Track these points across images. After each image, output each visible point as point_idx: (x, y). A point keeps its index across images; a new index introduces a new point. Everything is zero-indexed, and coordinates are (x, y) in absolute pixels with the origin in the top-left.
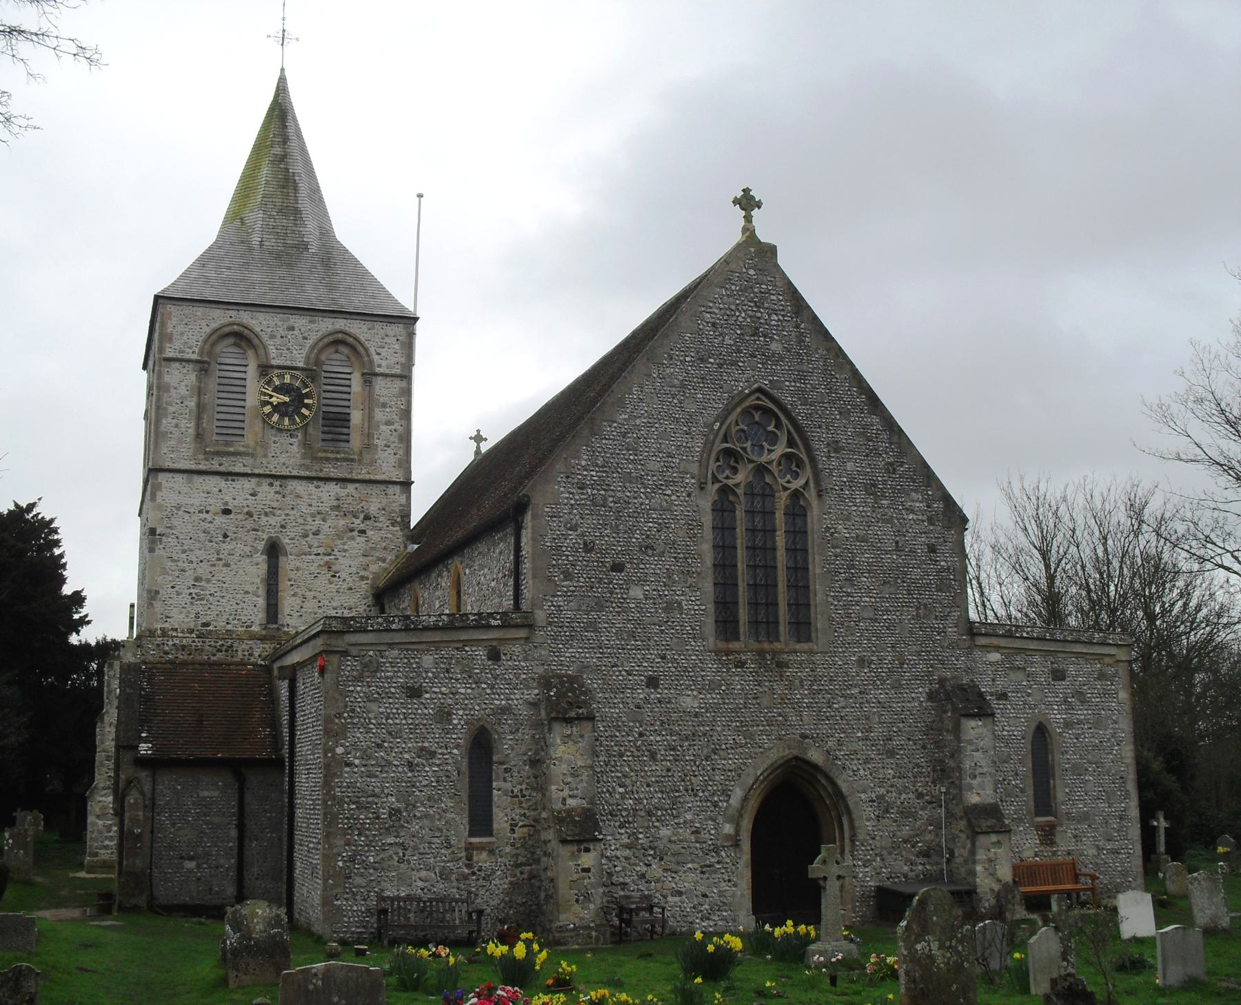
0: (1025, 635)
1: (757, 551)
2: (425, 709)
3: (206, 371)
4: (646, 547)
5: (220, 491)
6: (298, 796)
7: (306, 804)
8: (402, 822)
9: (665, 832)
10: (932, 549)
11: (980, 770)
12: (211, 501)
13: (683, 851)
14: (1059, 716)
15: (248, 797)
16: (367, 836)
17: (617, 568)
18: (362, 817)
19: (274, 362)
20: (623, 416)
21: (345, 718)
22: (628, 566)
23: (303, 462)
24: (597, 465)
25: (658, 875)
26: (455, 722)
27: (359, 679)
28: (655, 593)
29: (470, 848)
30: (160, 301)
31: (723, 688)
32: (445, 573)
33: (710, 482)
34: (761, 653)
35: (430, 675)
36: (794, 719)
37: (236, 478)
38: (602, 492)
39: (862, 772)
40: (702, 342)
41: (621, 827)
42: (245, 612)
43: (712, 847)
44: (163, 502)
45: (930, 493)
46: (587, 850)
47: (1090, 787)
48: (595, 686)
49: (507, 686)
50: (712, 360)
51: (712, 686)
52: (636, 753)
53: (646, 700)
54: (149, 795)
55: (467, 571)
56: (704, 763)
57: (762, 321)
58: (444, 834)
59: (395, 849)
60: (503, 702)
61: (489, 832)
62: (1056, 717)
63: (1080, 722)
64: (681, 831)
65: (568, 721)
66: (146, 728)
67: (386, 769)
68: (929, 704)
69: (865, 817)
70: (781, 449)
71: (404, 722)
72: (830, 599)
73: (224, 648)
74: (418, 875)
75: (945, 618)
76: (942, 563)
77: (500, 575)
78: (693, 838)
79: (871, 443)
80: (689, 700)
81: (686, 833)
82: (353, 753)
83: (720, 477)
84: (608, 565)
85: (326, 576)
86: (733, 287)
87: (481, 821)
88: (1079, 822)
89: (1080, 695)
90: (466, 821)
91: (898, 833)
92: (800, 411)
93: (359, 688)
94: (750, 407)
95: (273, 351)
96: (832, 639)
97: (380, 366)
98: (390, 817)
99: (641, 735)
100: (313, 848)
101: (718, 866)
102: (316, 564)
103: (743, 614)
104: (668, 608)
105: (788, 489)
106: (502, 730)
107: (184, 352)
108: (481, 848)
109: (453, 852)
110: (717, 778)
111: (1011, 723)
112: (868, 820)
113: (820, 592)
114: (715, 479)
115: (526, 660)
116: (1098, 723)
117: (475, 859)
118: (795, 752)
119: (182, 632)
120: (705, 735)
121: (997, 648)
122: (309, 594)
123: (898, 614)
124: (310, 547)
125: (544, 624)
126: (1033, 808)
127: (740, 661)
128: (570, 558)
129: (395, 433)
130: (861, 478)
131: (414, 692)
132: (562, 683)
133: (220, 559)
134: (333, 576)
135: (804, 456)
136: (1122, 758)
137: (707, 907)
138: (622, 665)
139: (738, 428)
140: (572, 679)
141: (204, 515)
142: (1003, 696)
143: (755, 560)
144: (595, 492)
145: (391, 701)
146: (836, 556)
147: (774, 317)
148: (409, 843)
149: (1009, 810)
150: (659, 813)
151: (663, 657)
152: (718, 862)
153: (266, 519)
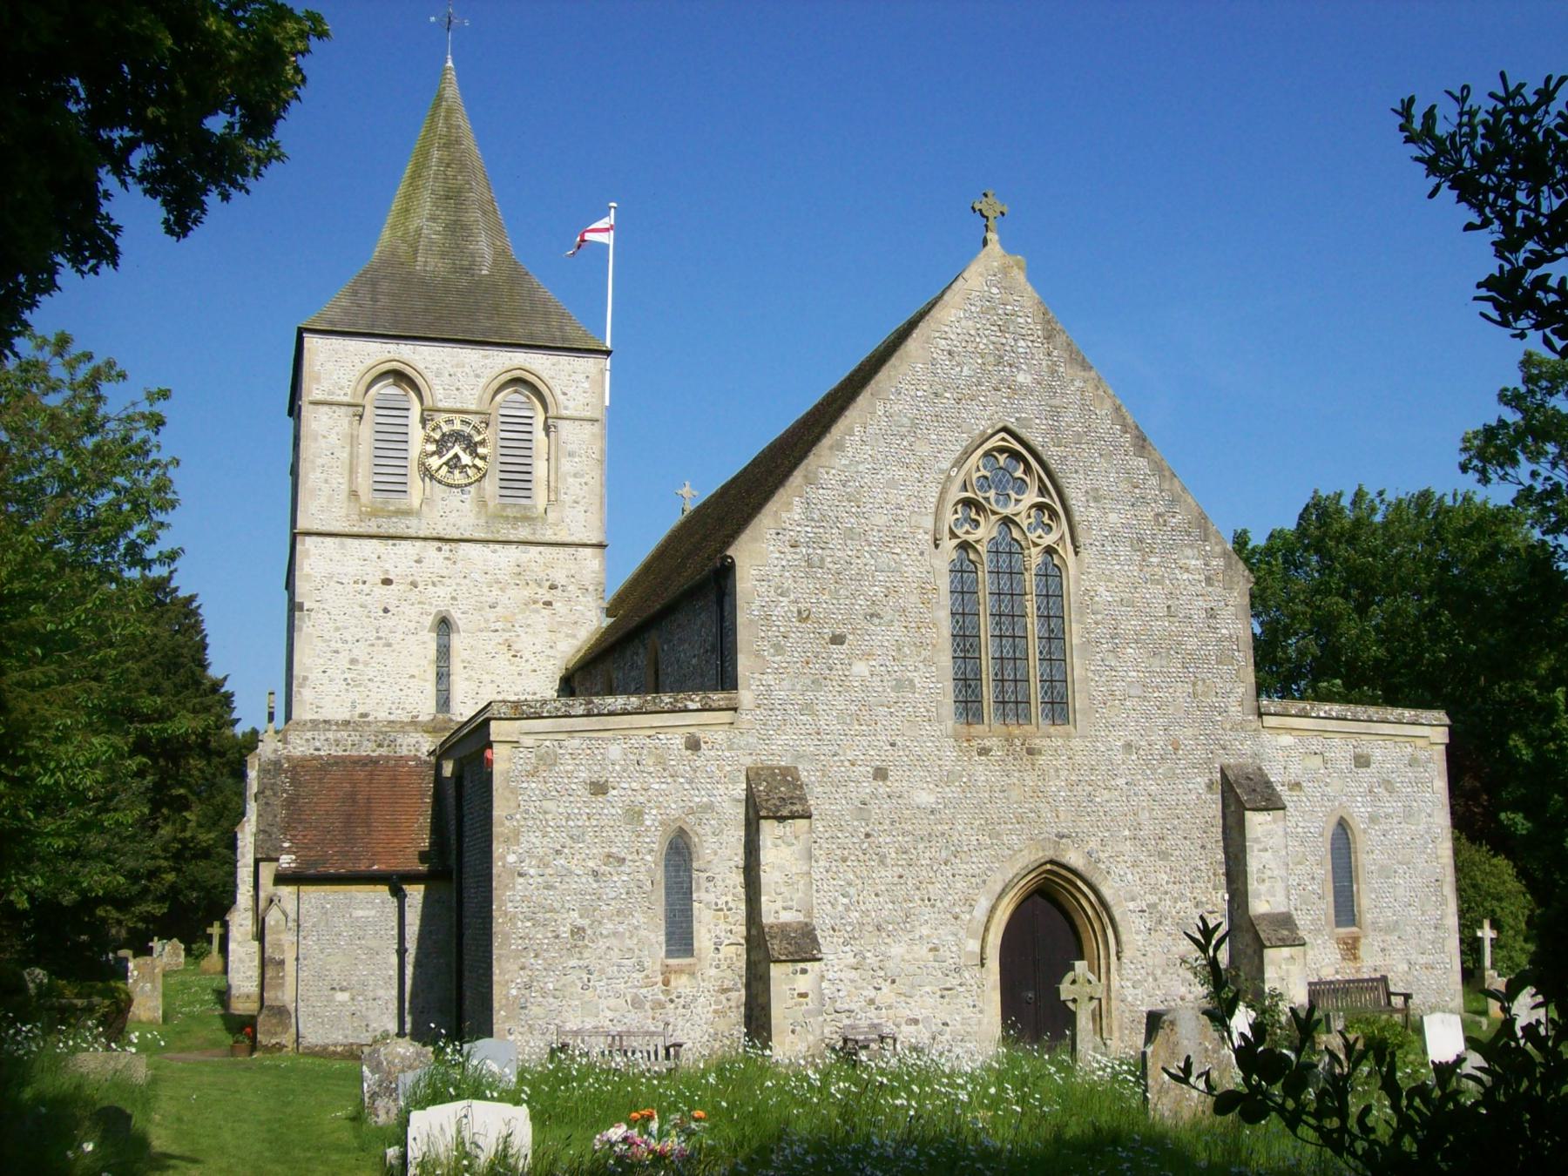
0: (1322, 714)
1: (1003, 619)
3: (361, 417)
4: (872, 615)
8: (586, 942)
9: (897, 950)
10: (1211, 614)
11: (1268, 873)
12: (369, 569)
13: (919, 971)
14: (1362, 810)
16: (545, 959)
17: (838, 640)
18: (540, 936)
19: (441, 405)
20: (843, 462)
21: (518, 821)
22: (851, 637)
23: (476, 522)
24: (813, 520)
25: (889, 1001)
26: (648, 823)
27: (533, 773)
29: (667, 972)
34: (1009, 739)
36: (1047, 814)
37: (397, 542)
38: (819, 551)
40: (935, 374)
41: (845, 944)
45: (1208, 548)
46: (804, 971)
47: (1400, 891)
48: (813, 779)
50: (947, 395)
51: (951, 778)
52: (862, 857)
53: (873, 795)
54: (293, 915)
55: (665, 647)
56: (943, 867)
57: (1008, 348)
59: (577, 972)
60: (705, 799)
62: (1358, 814)
63: (1387, 816)
64: (915, 947)
65: (782, 819)
68: (1209, 796)
69: (1133, 929)
70: (1031, 497)
72: (1090, 674)
73: (386, 743)
75: (1226, 695)
76: (1224, 631)
78: (931, 956)
79: (1137, 491)
80: (924, 794)
81: (922, 951)
82: (527, 861)
83: (959, 532)
85: (504, 658)
86: (973, 309)
87: (680, 938)
88: (1386, 933)
89: (1388, 784)
90: (662, 938)
92: (1052, 454)
93: (534, 785)
94: (994, 449)
95: (439, 393)
97: (566, 408)
98: (572, 935)
101: (961, 989)
102: (493, 643)
103: (988, 692)
104: (899, 685)
107: (333, 394)
108: (680, 971)
110: (958, 885)
111: (1306, 817)
112: (1138, 933)
113: (1078, 668)
114: (953, 535)
115: (730, 748)
116: (1408, 814)
117: (673, 984)
118: (1050, 854)
120: (943, 834)
121: (1290, 730)
122: (486, 678)
124: (487, 621)
125: (752, 706)
126: (1333, 918)
127: (983, 749)
128: (782, 629)
129: (585, 487)
130: (1126, 533)
131: (599, 788)
133: (379, 638)
135: (1058, 507)
136: (1437, 858)
138: (845, 755)
139: (979, 474)
140: (785, 771)
141: (361, 586)
142: (1296, 786)
144: (811, 551)
145: (571, 799)
146: (1096, 623)
147: (1021, 343)
148: (594, 964)
149: (1303, 921)
150: (890, 927)
151: (893, 745)
152: (961, 985)
153: (435, 589)
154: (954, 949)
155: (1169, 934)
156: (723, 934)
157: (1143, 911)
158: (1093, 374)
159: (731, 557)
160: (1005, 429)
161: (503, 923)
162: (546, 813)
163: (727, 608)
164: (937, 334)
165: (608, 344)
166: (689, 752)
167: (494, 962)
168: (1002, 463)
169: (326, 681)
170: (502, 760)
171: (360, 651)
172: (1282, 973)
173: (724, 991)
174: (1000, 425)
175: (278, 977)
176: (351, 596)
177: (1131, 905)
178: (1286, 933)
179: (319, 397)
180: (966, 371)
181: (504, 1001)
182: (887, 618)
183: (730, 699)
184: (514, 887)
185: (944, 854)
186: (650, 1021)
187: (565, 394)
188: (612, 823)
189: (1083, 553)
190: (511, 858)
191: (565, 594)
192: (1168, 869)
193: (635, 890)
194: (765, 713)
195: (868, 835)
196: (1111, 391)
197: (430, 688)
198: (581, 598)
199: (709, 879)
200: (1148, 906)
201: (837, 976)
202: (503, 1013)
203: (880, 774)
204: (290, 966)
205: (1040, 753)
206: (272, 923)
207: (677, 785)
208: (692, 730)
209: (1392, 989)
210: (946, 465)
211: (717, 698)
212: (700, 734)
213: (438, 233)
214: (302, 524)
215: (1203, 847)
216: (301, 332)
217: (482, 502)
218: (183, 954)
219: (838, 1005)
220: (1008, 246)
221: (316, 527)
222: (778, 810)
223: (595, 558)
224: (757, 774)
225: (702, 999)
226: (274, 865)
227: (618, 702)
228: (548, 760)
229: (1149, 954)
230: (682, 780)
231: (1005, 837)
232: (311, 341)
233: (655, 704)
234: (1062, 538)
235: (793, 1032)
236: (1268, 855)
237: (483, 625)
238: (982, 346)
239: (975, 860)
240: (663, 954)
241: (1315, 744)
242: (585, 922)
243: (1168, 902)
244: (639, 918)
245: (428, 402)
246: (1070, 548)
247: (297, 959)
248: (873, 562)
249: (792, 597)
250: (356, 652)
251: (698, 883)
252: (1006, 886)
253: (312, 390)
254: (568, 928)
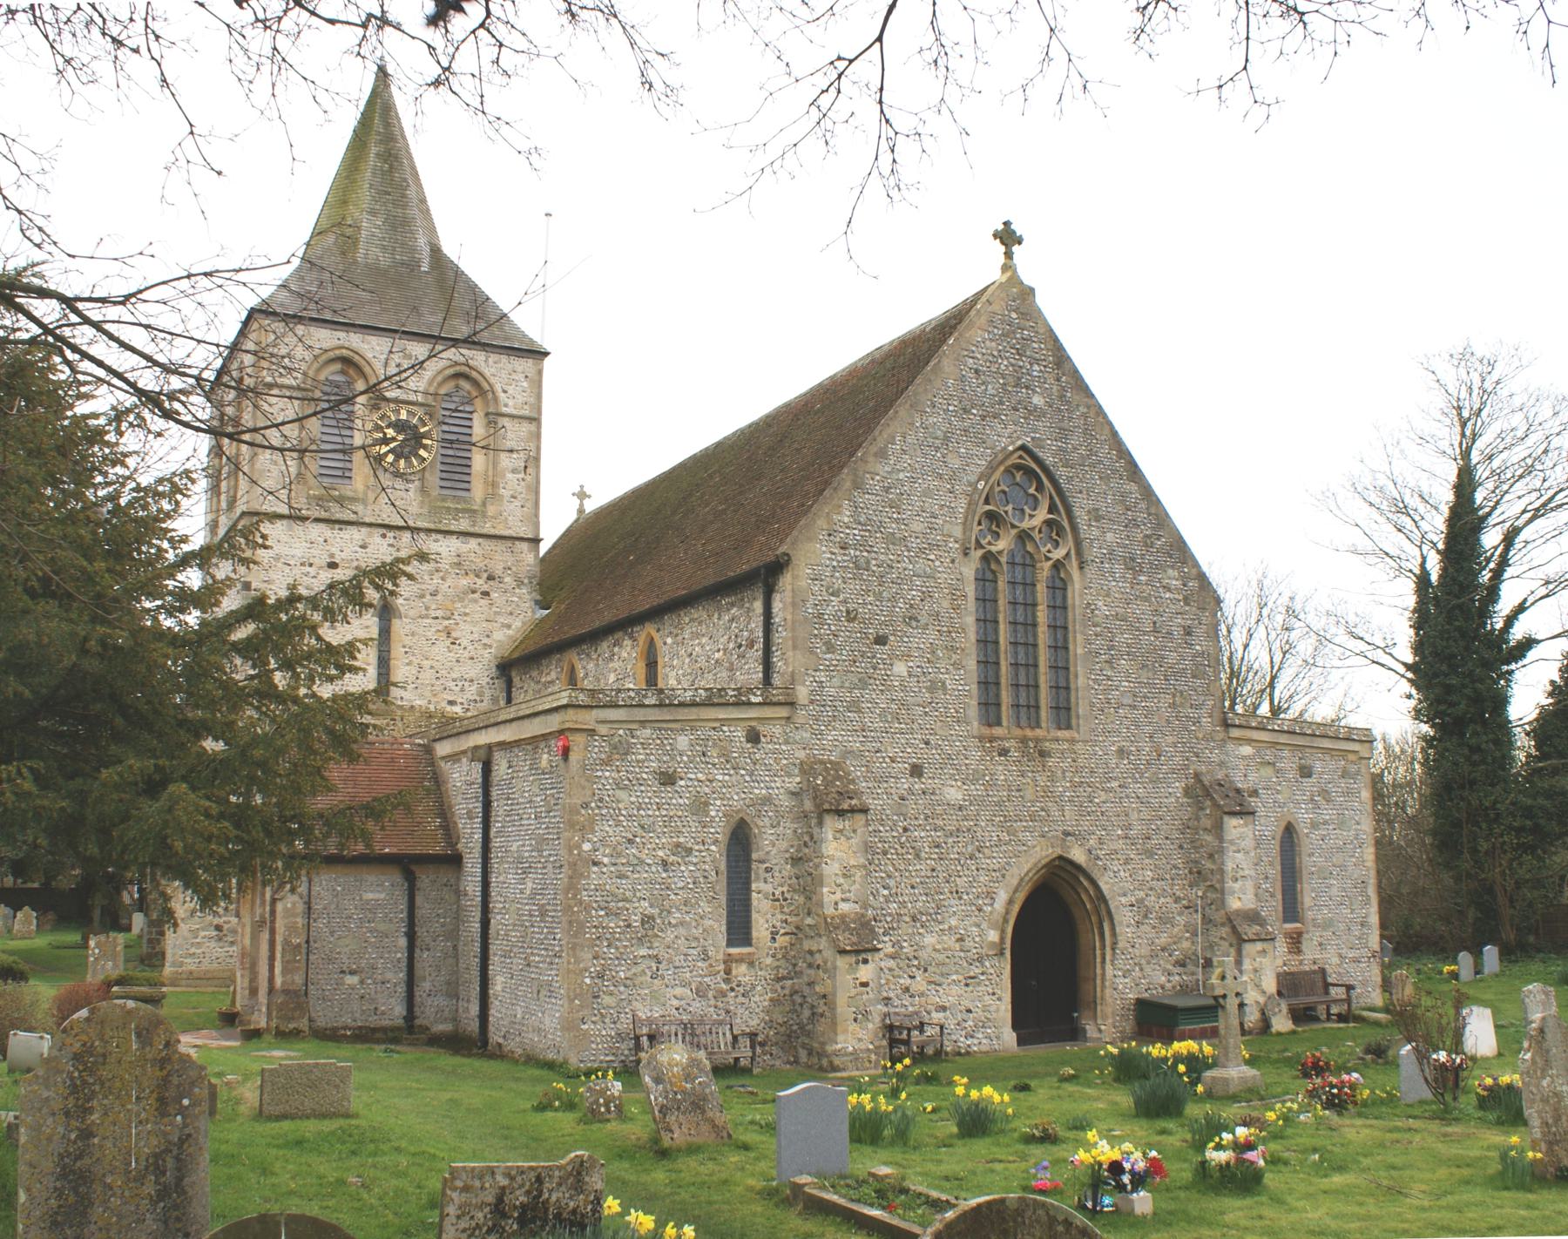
4: (910, 618)
9: (930, 940)
10: (1188, 632)
15: (419, 900)
16: (617, 948)
17: (881, 640)
18: (612, 925)
21: (592, 809)
22: (892, 638)
23: (420, 511)
27: (607, 763)
29: (729, 961)
30: (256, 315)
34: (1024, 741)
38: (865, 554)
46: (865, 961)
50: (974, 411)
55: (669, 640)
59: (647, 962)
60: (764, 791)
61: (747, 941)
62: (1303, 817)
63: (1325, 823)
65: (840, 813)
70: (1042, 514)
77: (731, 645)
78: (957, 946)
80: (952, 791)
81: (950, 941)
82: (602, 850)
83: (983, 542)
87: (739, 930)
89: (1324, 793)
90: (724, 928)
92: (1062, 473)
93: (607, 774)
97: (506, 405)
103: (1006, 697)
110: (982, 879)
113: (1082, 679)
115: (787, 742)
116: (1341, 825)
117: (734, 972)
118: (1059, 851)
121: (1249, 741)
122: (426, 663)
124: (427, 608)
125: (806, 702)
126: (1281, 915)
127: (1003, 749)
129: (522, 483)
130: (1120, 552)
131: (668, 779)
135: (1066, 524)
140: (837, 766)
141: (307, 569)
145: (643, 788)
147: (1036, 367)
148: (663, 954)
150: (924, 918)
151: (927, 743)
152: (982, 974)
154: (977, 939)
155: (1154, 927)
156: (779, 924)
157: (1133, 905)
162: (619, 801)
166: (749, 745)
168: (1018, 479)
172: (1256, 965)
173: (778, 979)
177: (1123, 900)
180: (991, 391)
182: (923, 622)
184: (589, 876)
185: (970, 849)
186: (712, 1009)
187: (505, 392)
195: (905, 830)
199: (768, 870)
200: (1137, 901)
203: (916, 771)
209: (1330, 980)
213: (378, 227)
215: (1181, 847)
217: (423, 490)
218: (35, 921)
222: (839, 805)
225: (759, 988)
228: (621, 750)
230: (743, 772)
231: (1020, 834)
234: (1068, 554)
235: (855, 1020)
237: (424, 612)
238: (1003, 367)
240: (722, 939)
242: (655, 911)
243: (1153, 898)
244: (705, 907)
246: (1075, 563)
248: (911, 567)
249: (842, 597)
251: (756, 874)
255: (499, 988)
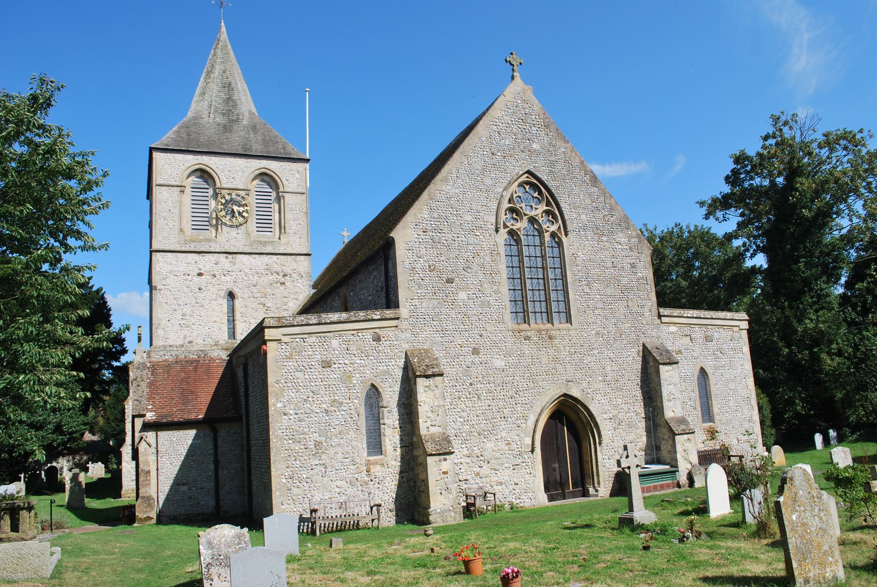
0: (689, 315)
2: (333, 375)
3: (183, 192)
5: (196, 262)
6: (253, 438)
7: (258, 443)
8: (323, 450)
9: (490, 445)
10: (633, 266)
13: (501, 456)
14: (711, 363)
17: (450, 281)
18: (297, 448)
19: (225, 186)
22: (457, 279)
28: (474, 295)
29: (368, 464)
31: (519, 353)
32: (337, 298)
33: (502, 227)
35: (337, 352)
38: (438, 234)
39: (603, 401)
42: (214, 333)
43: (518, 453)
44: (160, 270)
45: (630, 233)
46: (445, 460)
49: (386, 357)
50: (499, 154)
53: (473, 363)
55: (352, 294)
56: (510, 400)
58: (351, 456)
64: (499, 443)
66: (151, 403)
67: (311, 415)
71: (321, 384)
74: (335, 484)
75: (643, 306)
76: (640, 274)
79: (594, 204)
80: (498, 361)
81: (502, 445)
82: (288, 406)
83: (508, 224)
84: (444, 279)
87: (376, 445)
90: (365, 446)
91: (627, 437)
93: (290, 364)
96: (580, 321)
99: (471, 384)
100: (264, 472)
101: (523, 465)
105: (548, 231)
106: (384, 386)
108: (376, 463)
109: (358, 468)
110: (519, 409)
114: (505, 226)
117: (372, 470)
119: (176, 347)
123: (617, 305)
131: (326, 364)
132: (420, 353)
133: (197, 303)
134: (266, 310)
137: (519, 491)
138: (457, 342)
139: (516, 195)
141: (187, 277)
143: (531, 275)
154: (518, 443)
157: (611, 419)
158: (569, 144)
159: (392, 237)
160: (529, 172)
161: (276, 442)
163: (390, 266)
164: (492, 123)
165: (308, 156)
166: (375, 343)
167: (272, 465)
169: (170, 325)
170: (272, 350)
171: (187, 310)
174: (526, 170)
175: (147, 480)
176: (182, 282)
177: (605, 416)
178: (684, 426)
179: (162, 182)
181: (278, 487)
183: (396, 313)
184: (281, 421)
186: (360, 492)
187: (287, 180)
188: (335, 383)
189: (570, 235)
190: (279, 405)
191: (291, 278)
192: (621, 397)
193: (349, 419)
194: (415, 320)
195: (471, 384)
196: (579, 154)
197: (225, 328)
198: (299, 280)
201: (459, 461)
202: (278, 493)
204: (153, 474)
205: (555, 339)
206: (143, 450)
207: (369, 361)
208: (376, 330)
210: (500, 190)
211: (389, 313)
212: (380, 332)
214: (154, 247)
216: (151, 150)
219: (461, 478)
220: (526, 81)
221: (161, 248)
222: (426, 372)
223: (306, 261)
224: (412, 353)
226: (142, 419)
227: (335, 316)
229: (615, 441)
230: (372, 358)
232: (155, 155)
233: (356, 317)
234: (559, 228)
236: (671, 387)
239: (526, 395)
240: (366, 454)
241: (687, 330)
245: (218, 185)
247: (157, 470)
250: (185, 310)
251: (383, 414)
252: (543, 408)
253: (157, 179)
254: (312, 443)
255: (254, 488)
